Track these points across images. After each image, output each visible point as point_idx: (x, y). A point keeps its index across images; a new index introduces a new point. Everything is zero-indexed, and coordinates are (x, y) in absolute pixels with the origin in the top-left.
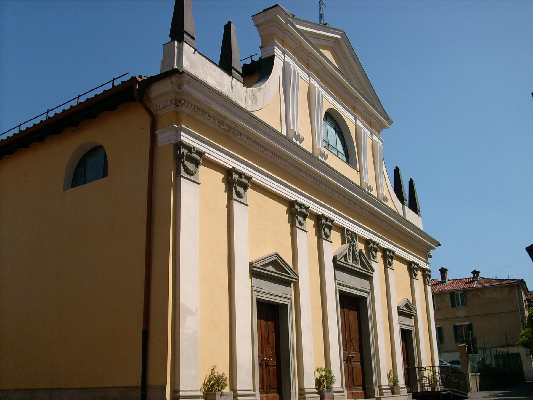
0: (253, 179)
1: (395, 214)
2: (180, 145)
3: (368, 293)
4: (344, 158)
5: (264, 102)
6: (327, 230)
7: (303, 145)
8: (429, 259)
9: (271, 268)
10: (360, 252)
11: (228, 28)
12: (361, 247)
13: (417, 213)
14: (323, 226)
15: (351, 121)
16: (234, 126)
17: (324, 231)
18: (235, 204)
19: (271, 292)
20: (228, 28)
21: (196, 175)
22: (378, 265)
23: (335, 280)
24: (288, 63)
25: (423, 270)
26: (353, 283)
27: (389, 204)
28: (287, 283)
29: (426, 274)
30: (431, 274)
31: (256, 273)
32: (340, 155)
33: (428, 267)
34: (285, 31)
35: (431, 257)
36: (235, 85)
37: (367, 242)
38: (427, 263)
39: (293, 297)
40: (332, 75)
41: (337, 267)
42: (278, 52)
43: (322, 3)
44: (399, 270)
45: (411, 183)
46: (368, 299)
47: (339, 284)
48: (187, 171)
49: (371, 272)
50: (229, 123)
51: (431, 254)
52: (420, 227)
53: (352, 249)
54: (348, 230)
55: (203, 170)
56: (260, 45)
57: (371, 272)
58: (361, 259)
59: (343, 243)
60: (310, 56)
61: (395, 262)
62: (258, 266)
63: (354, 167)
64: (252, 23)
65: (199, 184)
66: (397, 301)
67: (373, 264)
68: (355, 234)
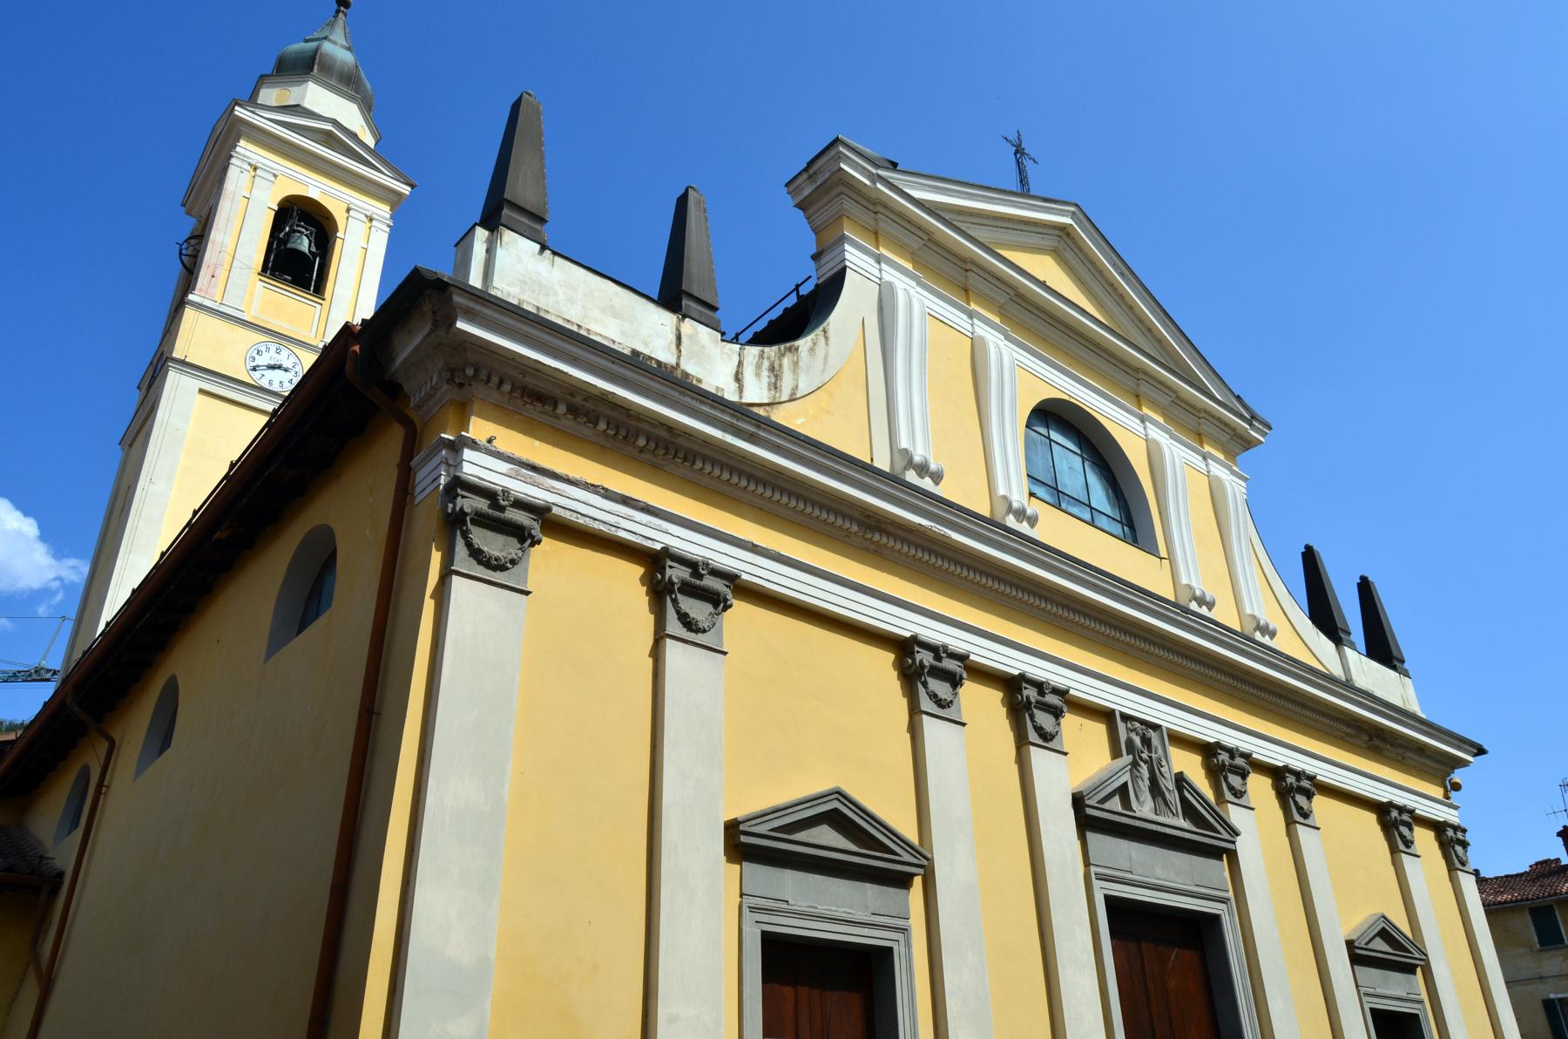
0: (1072, 692)
1: (636, 367)
2: (459, 485)
3: (1224, 901)
4: (1117, 529)
5: (825, 394)
6: (1404, 830)
7: (1214, 614)
8: (1453, 794)
9: (825, 836)
10: (1180, 780)
11: (682, 203)
12: (1189, 765)
13: (1394, 668)
14: (1031, 708)
15: (1132, 430)
16: (665, 434)
17: (1032, 720)
18: (1300, 829)
19: (822, 909)
20: (682, 203)
21: (953, 708)
22: (1255, 820)
23: (1087, 864)
24: (1218, 478)
25: (1438, 828)
26: (1159, 871)
27: (1284, 643)
28: (1409, 969)
29: (1450, 840)
30: (1468, 837)
31: (1358, 957)
32: (1102, 521)
33: (1450, 816)
34: (875, 206)
35: (1456, 787)
36: (691, 337)
37: (1208, 751)
38: (1446, 801)
39: (1424, 996)
40: (1219, 419)
41: (1087, 821)
42: (853, 256)
43: (1023, 154)
44: (1343, 836)
45: (1365, 589)
46: (1226, 920)
47: (1101, 877)
48: (687, 622)
49: (1226, 836)
50: (647, 427)
51: (1457, 780)
52: (1415, 707)
53: (1146, 774)
54: (1126, 718)
55: (1071, 723)
56: (814, 251)
57: (1226, 836)
58: (1183, 800)
59: (1116, 754)
60: (968, 266)
61: (1321, 806)
62: (763, 829)
63: (1152, 550)
64: (790, 202)
65: (527, 593)
66: (1340, 926)
67: (1235, 815)
68: (1156, 727)
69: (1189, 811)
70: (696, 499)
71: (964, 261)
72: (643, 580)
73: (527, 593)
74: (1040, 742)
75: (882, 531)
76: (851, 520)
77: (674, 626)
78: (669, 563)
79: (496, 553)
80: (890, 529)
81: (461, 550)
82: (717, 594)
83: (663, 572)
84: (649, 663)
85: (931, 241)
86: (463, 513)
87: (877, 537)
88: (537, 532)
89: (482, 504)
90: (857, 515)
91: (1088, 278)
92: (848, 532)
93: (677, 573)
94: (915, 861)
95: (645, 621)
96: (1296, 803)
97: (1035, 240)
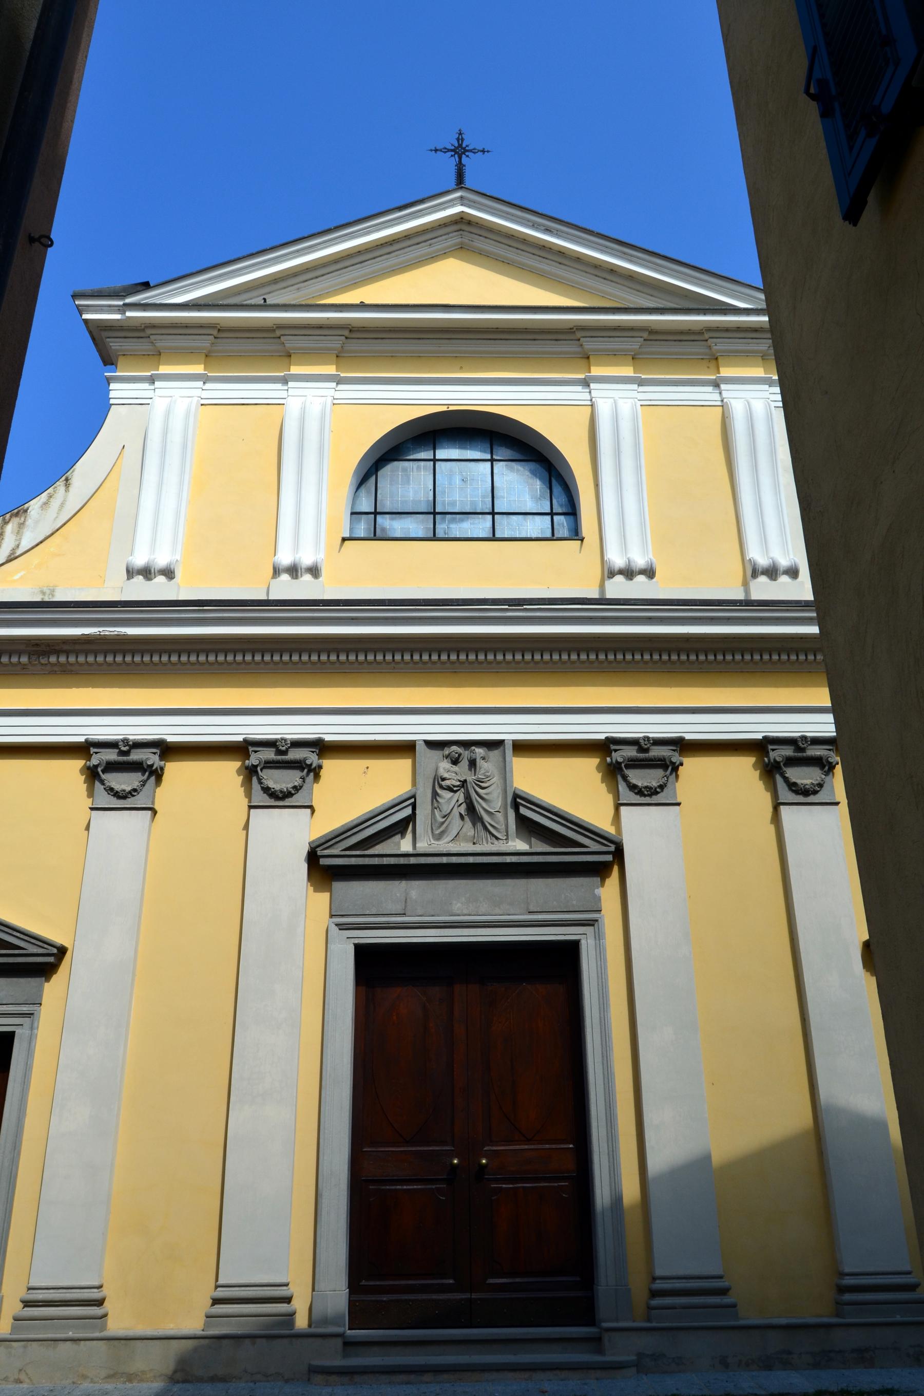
26: (457, 906)
48: (793, 787)
60: (278, 333)
65: (679, 804)
69: (527, 827)
70: (493, 686)
71: (700, 333)
72: (755, 766)
73: (679, 804)
74: (273, 802)
75: (58, 653)
76: (20, 654)
77: (785, 795)
78: (770, 747)
79: (808, 782)
80: (66, 647)
81: (622, 787)
82: (662, 759)
83: (768, 756)
84: (772, 828)
85: (220, 331)
86: (619, 763)
87: (53, 659)
88: (676, 758)
89: (788, 752)
90: (22, 647)
91: (511, 254)
92: (24, 667)
93: (778, 754)
94: (41, 951)
95: (764, 799)
96: (786, 780)
97: (424, 250)
